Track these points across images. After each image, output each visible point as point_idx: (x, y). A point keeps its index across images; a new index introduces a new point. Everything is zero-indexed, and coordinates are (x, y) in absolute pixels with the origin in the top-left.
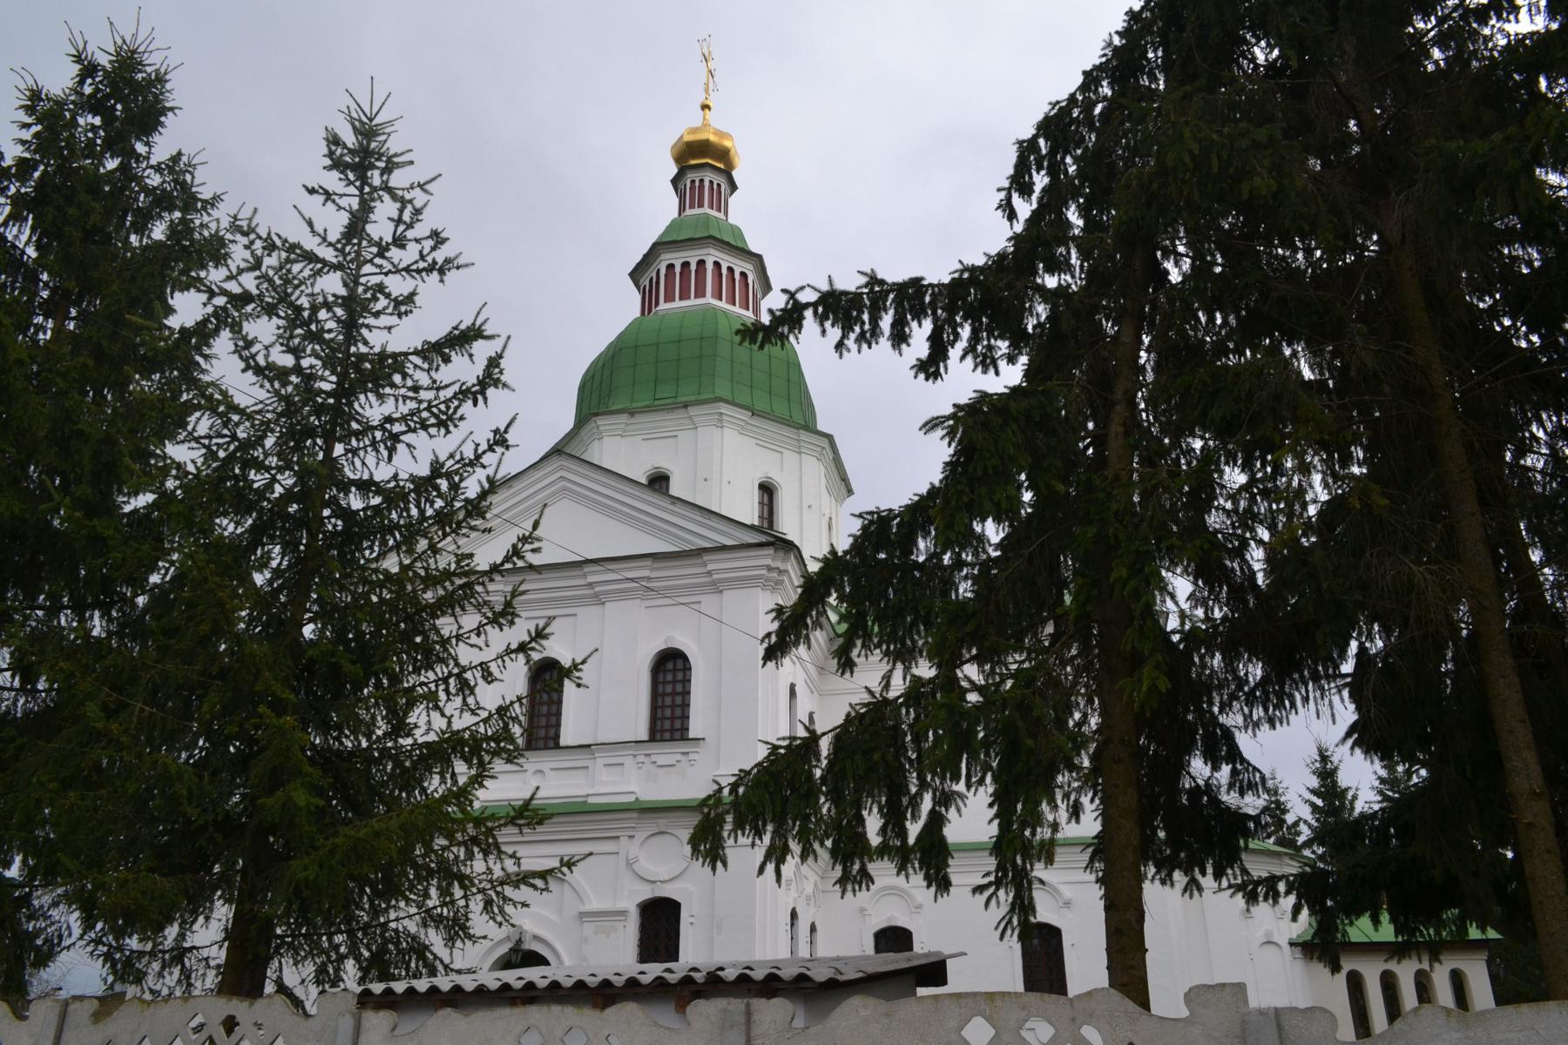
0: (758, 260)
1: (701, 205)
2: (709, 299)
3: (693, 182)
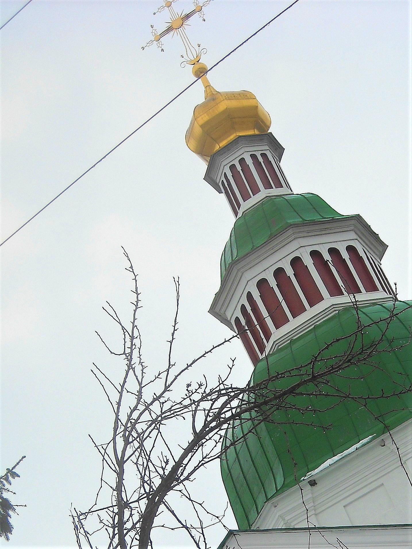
0: (358, 223)
1: (256, 191)
2: (328, 301)
3: (233, 168)
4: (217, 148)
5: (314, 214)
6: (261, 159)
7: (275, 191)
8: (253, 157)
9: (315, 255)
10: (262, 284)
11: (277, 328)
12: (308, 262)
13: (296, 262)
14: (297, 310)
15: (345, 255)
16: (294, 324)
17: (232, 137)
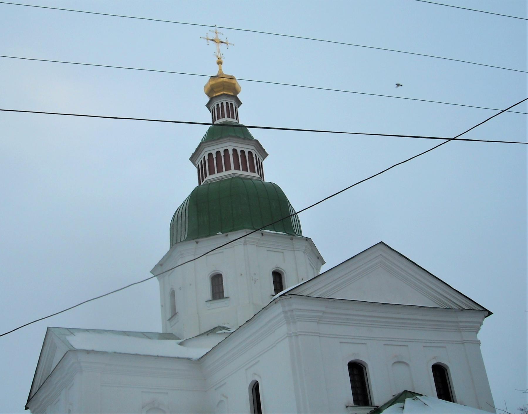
2: (233, 171)
3: (218, 105)
4: (215, 95)
5: (241, 132)
6: (230, 105)
7: (231, 120)
8: (227, 103)
9: (235, 151)
10: (210, 155)
11: (210, 175)
12: (231, 152)
13: (226, 151)
14: (220, 170)
15: (247, 155)
16: (217, 175)
17: (222, 93)
